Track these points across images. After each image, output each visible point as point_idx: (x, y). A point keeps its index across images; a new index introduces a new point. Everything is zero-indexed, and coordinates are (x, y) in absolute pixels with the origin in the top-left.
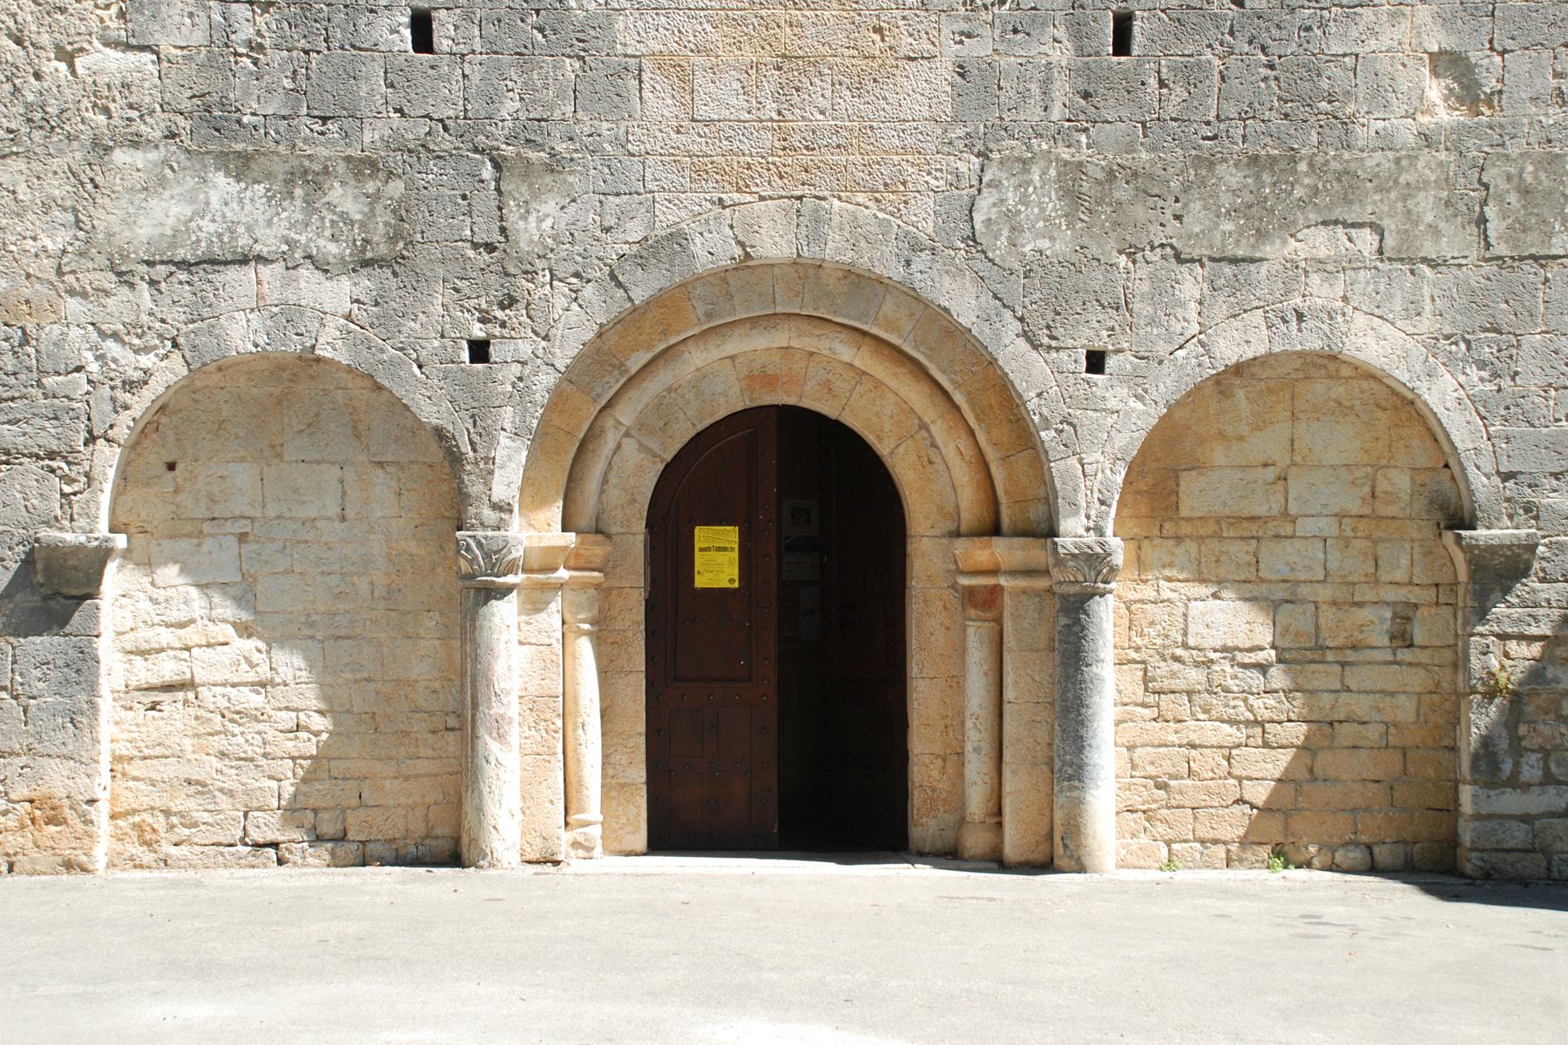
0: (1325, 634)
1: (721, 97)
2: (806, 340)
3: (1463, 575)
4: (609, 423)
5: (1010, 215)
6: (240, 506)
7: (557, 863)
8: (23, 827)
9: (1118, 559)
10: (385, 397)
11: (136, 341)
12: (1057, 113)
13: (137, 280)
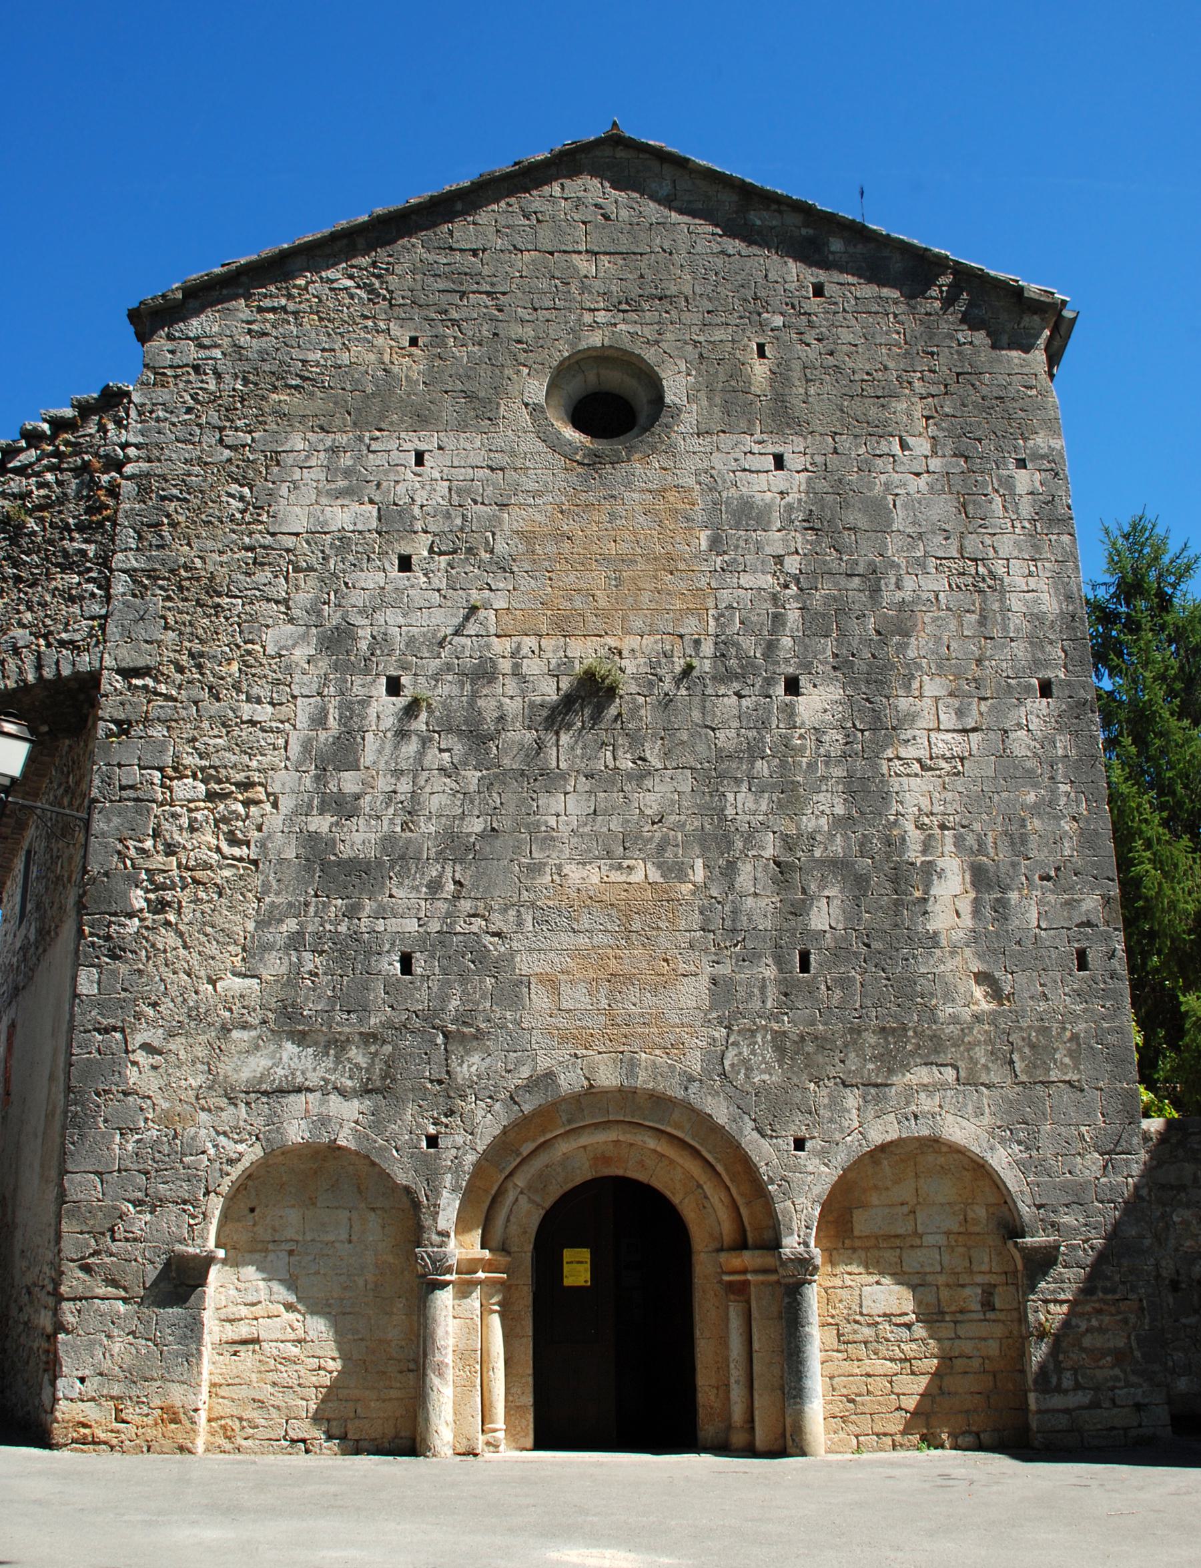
0: (943, 1304)
1: (575, 997)
2: (628, 1136)
3: (1020, 1266)
4: (510, 1185)
5: (745, 1062)
6: (290, 1233)
7: (476, 1455)
8: (156, 1424)
9: (818, 1261)
10: (377, 1169)
11: (236, 1137)
12: (769, 1005)
13: (239, 1102)
